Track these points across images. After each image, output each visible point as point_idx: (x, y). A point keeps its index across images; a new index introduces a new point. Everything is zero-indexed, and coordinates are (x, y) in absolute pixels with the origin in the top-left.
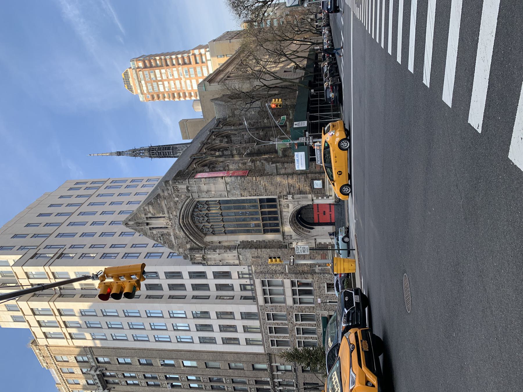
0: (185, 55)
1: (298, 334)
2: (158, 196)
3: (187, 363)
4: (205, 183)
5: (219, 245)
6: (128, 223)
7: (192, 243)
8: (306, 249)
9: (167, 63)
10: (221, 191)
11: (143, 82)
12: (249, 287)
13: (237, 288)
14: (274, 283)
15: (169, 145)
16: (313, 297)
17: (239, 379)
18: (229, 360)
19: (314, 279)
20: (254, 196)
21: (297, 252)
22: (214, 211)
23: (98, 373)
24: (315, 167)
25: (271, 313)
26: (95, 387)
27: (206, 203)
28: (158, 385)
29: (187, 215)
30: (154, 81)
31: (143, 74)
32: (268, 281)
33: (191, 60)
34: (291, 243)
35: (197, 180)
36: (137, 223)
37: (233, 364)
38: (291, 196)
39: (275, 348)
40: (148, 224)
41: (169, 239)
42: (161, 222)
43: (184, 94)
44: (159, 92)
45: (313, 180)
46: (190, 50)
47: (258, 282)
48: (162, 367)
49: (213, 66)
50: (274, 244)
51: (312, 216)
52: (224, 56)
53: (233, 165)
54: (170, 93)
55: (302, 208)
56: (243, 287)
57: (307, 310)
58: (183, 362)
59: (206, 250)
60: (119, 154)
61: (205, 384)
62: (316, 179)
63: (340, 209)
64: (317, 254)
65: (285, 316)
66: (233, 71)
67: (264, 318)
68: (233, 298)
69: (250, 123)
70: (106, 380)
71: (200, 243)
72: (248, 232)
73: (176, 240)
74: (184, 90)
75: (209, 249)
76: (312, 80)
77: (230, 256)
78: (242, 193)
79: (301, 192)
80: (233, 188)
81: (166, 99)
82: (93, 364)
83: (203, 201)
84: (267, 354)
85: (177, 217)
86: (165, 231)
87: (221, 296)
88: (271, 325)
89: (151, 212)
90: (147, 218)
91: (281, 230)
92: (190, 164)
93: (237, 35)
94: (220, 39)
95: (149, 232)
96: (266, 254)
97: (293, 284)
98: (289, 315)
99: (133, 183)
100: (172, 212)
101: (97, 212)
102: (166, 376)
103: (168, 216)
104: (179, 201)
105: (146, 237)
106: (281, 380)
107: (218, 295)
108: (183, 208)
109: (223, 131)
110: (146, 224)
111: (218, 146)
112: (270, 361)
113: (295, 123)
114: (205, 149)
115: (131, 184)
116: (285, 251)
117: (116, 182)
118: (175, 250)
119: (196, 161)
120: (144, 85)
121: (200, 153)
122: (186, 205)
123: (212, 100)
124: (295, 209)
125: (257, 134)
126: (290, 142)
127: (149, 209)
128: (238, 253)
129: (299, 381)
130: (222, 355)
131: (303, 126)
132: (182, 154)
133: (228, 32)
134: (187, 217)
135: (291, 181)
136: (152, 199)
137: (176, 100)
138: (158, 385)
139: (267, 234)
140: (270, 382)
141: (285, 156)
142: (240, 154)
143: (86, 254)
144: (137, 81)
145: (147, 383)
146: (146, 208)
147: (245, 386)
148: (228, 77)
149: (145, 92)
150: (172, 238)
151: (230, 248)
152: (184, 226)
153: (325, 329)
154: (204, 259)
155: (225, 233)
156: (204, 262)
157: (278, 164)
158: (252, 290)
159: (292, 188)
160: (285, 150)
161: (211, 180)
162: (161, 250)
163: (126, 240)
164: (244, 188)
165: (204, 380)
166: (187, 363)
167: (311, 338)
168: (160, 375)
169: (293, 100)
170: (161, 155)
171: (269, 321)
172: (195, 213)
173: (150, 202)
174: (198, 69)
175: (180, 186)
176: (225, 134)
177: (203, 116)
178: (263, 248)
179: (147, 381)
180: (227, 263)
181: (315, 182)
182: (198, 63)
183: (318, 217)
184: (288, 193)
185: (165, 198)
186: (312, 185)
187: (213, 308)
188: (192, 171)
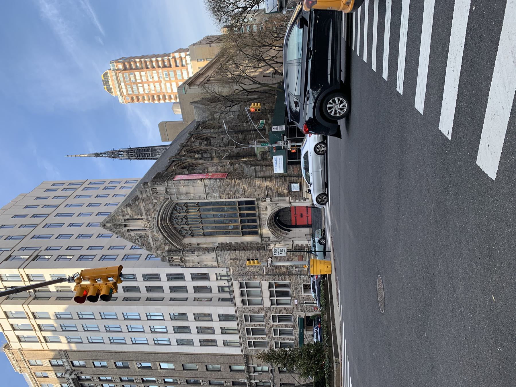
1: (275, 335)
2: (137, 198)
3: (164, 365)
4: (184, 185)
7: (171, 245)
9: (147, 66)
10: (200, 193)
11: (123, 84)
12: (227, 289)
13: (215, 290)
14: (252, 285)
15: (148, 147)
16: (290, 298)
17: (216, 381)
19: (291, 280)
20: (233, 198)
21: (275, 253)
22: (193, 213)
23: (73, 376)
24: (293, 170)
25: (249, 314)
27: (184, 205)
32: (246, 282)
33: (171, 63)
34: (269, 245)
36: (115, 225)
39: (252, 349)
40: (125, 226)
41: (147, 241)
42: (140, 224)
45: (291, 183)
46: (170, 53)
48: (139, 370)
49: (193, 69)
52: (204, 59)
53: (213, 167)
56: (221, 289)
58: (160, 364)
59: (184, 252)
60: (98, 155)
64: (294, 255)
66: (213, 74)
67: (241, 320)
68: (211, 299)
72: (226, 234)
73: (154, 242)
74: (163, 93)
77: (209, 258)
79: (279, 195)
81: (146, 102)
82: (68, 368)
85: (156, 219)
86: (143, 233)
87: (199, 298)
88: (248, 326)
90: (125, 220)
91: (259, 232)
92: (170, 166)
94: (200, 43)
95: (127, 234)
97: (270, 285)
98: (267, 316)
101: (74, 213)
102: (142, 379)
103: (146, 218)
104: (158, 203)
105: (124, 238)
106: (257, 381)
107: (196, 297)
108: (162, 210)
109: (202, 134)
110: (123, 226)
113: (273, 127)
115: (110, 185)
116: (263, 253)
117: (94, 183)
120: (124, 87)
121: (179, 155)
122: (165, 207)
123: (192, 103)
125: (237, 137)
128: (216, 255)
133: (208, 36)
134: (165, 219)
136: (130, 201)
139: (245, 236)
140: (247, 383)
141: (263, 159)
142: (219, 157)
144: (116, 82)
148: (208, 80)
149: (125, 94)
150: (150, 240)
151: (209, 250)
152: (163, 228)
153: (301, 330)
154: (182, 261)
155: (204, 235)
156: (183, 264)
157: (256, 167)
158: (230, 292)
159: (270, 191)
160: (263, 154)
161: (191, 182)
162: (139, 252)
163: (105, 242)
164: (223, 190)
165: (181, 382)
166: (164, 365)
167: (288, 338)
169: (271, 105)
170: (140, 157)
171: (247, 323)
173: (128, 203)
174: (178, 72)
177: (183, 118)
178: (241, 250)
179: (123, 384)
182: (178, 67)
183: (296, 219)
184: (266, 195)
185: (144, 200)
186: (289, 188)
187: (190, 310)
188: (171, 174)
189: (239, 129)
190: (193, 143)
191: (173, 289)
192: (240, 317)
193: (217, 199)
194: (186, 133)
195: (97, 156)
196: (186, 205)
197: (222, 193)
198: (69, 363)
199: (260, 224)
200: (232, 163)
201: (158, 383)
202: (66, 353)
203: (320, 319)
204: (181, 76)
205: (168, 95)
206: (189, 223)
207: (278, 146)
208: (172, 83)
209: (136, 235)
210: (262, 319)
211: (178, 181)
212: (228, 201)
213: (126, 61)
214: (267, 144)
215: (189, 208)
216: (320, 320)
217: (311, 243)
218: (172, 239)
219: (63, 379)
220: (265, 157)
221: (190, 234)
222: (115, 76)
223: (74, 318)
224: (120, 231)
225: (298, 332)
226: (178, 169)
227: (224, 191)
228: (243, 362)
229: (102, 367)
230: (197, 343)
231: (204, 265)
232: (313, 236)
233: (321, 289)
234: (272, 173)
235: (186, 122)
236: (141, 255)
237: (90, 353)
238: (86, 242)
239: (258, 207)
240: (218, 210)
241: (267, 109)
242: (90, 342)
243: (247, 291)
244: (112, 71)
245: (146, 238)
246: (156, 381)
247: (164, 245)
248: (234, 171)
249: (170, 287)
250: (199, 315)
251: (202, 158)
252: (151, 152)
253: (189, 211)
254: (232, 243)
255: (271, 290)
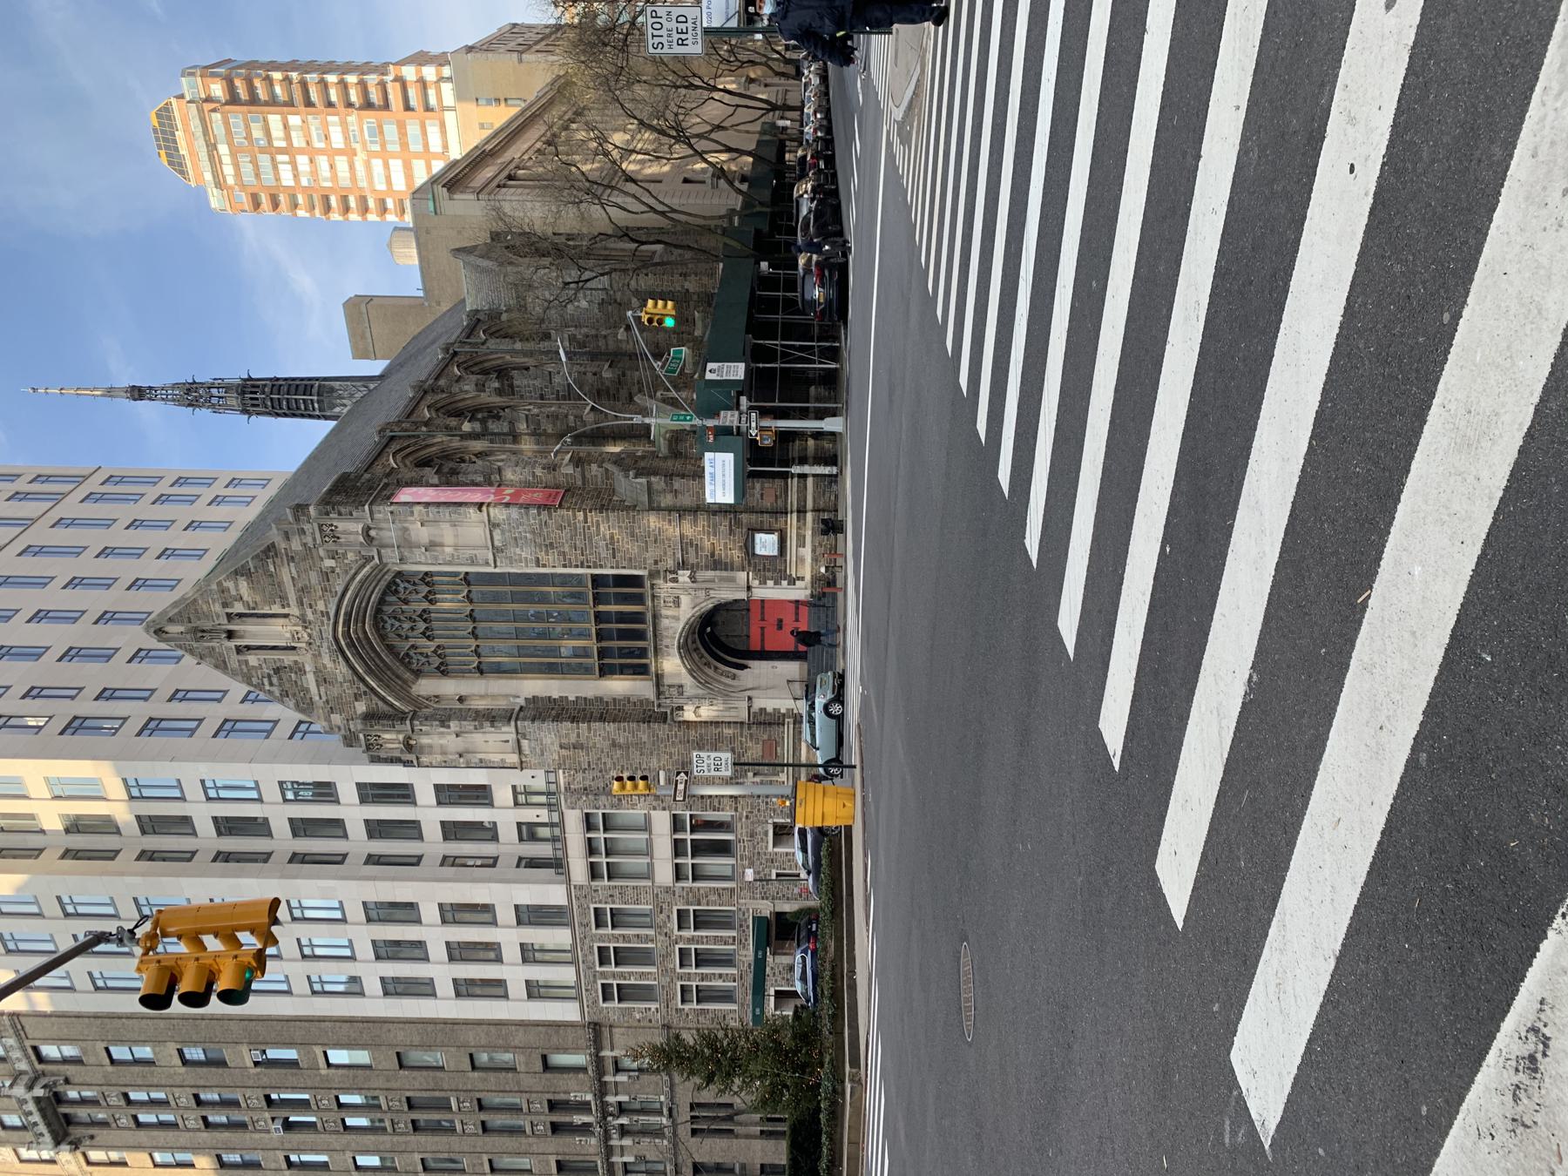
0: (372, 79)
1: (682, 965)
2: (270, 550)
3: (338, 1056)
4: (425, 518)
5: (459, 706)
6: (166, 629)
7: (373, 697)
8: (690, 25)
9: (309, 97)
10: (474, 547)
11: (223, 149)
12: (544, 832)
13: (508, 833)
14: (619, 821)
15: (310, 379)
16: (731, 861)
17: (497, 1099)
18: (473, 1044)
19: (739, 809)
20: (577, 566)
21: (699, 769)
22: (448, 603)
23: (39, 1092)
24: (762, 495)
25: (608, 907)
26: (29, 1136)
27: (422, 579)
28: (242, 1126)
29: (361, 614)
30: (262, 151)
31: (226, 123)
32: (604, 814)
33: (391, 97)
34: (681, 708)
35: (401, 509)
36: (196, 630)
37: (486, 1055)
38: (688, 573)
39: (606, 932)
40: (231, 635)
41: (299, 683)
42: (277, 632)
43: (363, 201)
44: (279, 187)
45: (754, 530)
46: (387, 64)
47: (573, 819)
48: (258, 1070)
49: (462, 128)
50: (629, 707)
51: (745, 633)
52: (498, 100)
53: (517, 469)
54: (315, 196)
55: (721, 608)
56: (528, 832)
57: (713, 898)
58: (325, 1053)
59: (416, 722)
60: (138, 393)
61: (394, 1116)
62: (761, 530)
63: (823, 617)
64: (751, 740)
65: (646, 915)
66: (526, 157)
67: (585, 922)
68: (493, 862)
69: (575, 335)
70: (66, 1116)
71: (398, 699)
72: (552, 670)
73: (322, 689)
74: (360, 189)
75: (426, 719)
76: (766, 229)
77: (494, 742)
78: (542, 555)
79: (717, 564)
80: (513, 542)
81: (301, 213)
82: (23, 1066)
83: (415, 572)
84: (589, 1023)
85: (329, 619)
86: (288, 659)
87: (456, 857)
88: (604, 941)
89: (245, 598)
90: (229, 616)
91: (653, 669)
92: (379, 454)
93: (542, 39)
94: (486, 47)
95: (233, 661)
96: (604, 739)
97: (677, 823)
98: (661, 912)
99: (182, 488)
100: (313, 603)
101: (53, 578)
102: (267, 1098)
103: (297, 613)
104: (338, 570)
105: (225, 673)
106: (624, 1098)
107: (448, 853)
108: (350, 592)
109: (486, 354)
110: (224, 635)
111: (469, 402)
112: (597, 1043)
113: (710, 366)
114: (429, 407)
115: (176, 490)
116: (662, 730)
117: (122, 480)
118: (319, 717)
119: (398, 448)
120: (226, 160)
121: (413, 418)
122: (359, 582)
123: (458, 251)
124: (698, 611)
125: (595, 374)
126: (692, 423)
127: (237, 590)
128: (517, 733)
129: (676, 1100)
130: (474, 1147)
131: (732, 378)
132: (349, 411)
133: (515, 25)
134: (360, 618)
135: (688, 529)
136: (249, 559)
137: (332, 219)
138: (242, 1126)
139: (609, 679)
140: (593, 1103)
141: (675, 454)
142: (540, 435)
143: (11, 717)
144: (201, 142)
145: (205, 1119)
146: (230, 584)
147: (518, 1119)
148: (510, 178)
149: (230, 181)
150: (310, 681)
151: (494, 717)
152: (351, 645)
153: (760, 953)
154: (409, 747)
155: (480, 671)
156: (410, 754)
157: (653, 479)
158: (554, 839)
159: (692, 551)
160: (677, 437)
161: (445, 511)
162: (273, 710)
163: (158, 675)
164: (547, 542)
165: (391, 1104)
166: (338, 1056)
167: (720, 976)
168: (248, 1093)
169: (705, 280)
170: (281, 408)
171: (601, 931)
172: (385, 608)
173: (242, 566)
174: (413, 129)
175: (342, 526)
176: (494, 362)
177: (425, 289)
178: (595, 721)
179: (204, 1113)
180: (481, 761)
181: (760, 538)
182: (413, 110)
183: (763, 635)
184: (679, 563)
185: (292, 557)
186: (749, 547)
187: (429, 894)
188: (385, 480)
189: (603, 347)
190: (457, 381)
191: (376, 829)
192: (580, 915)
193: (527, 566)
194: (433, 342)
195: (137, 396)
196: (428, 579)
197: (544, 549)
198: (24, 1049)
199: (655, 648)
200: (580, 458)
201: (316, 1108)
202: (16, 1021)
203: (814, 926)
204: (421, 141)
205: (375, 200)
206: (435, 632)
207: (721, 424)
208: (391, 162)
209: (264, 665)
210: (648, 919)
211: (407, 508)
212: (561, 575)
213: (238, 75)
214: (688, 418)
215: (437, 588)
216: (814, 929)
217: (802, 707)
218: (379, 679)
219: (5, 1099)
220: (681, 447)
221: (436, 665)
222: (197, 121)
223: (77, 988)
224: (213, 648)
225: (751, 958)
226: (406, 466)
227: (551, 544)
228: (582, 1043)
229: (137, 1062)
230: (445, 988)
231: (477, 761)
232: (809, 693)
233: (823, 862)
234: (698, 498)
235: (434, 304)
236: (276, 722)
237: (99, 1021)
238: (93, 675)
239: (653, 596)
240: (528, 598)
241: (691, 290)
242: (97, 989)
243: (605, 839)
244: (189, 102)
245: (296, 673)
246: (313, 1102)
247: (352, 699)
248: (584, 484)
249: (367, 821)
250: (462, 945)
251: (484, 435)
252: (318, 395)
253: (438, 596)
254: (567, 697)
255: (679, 836)
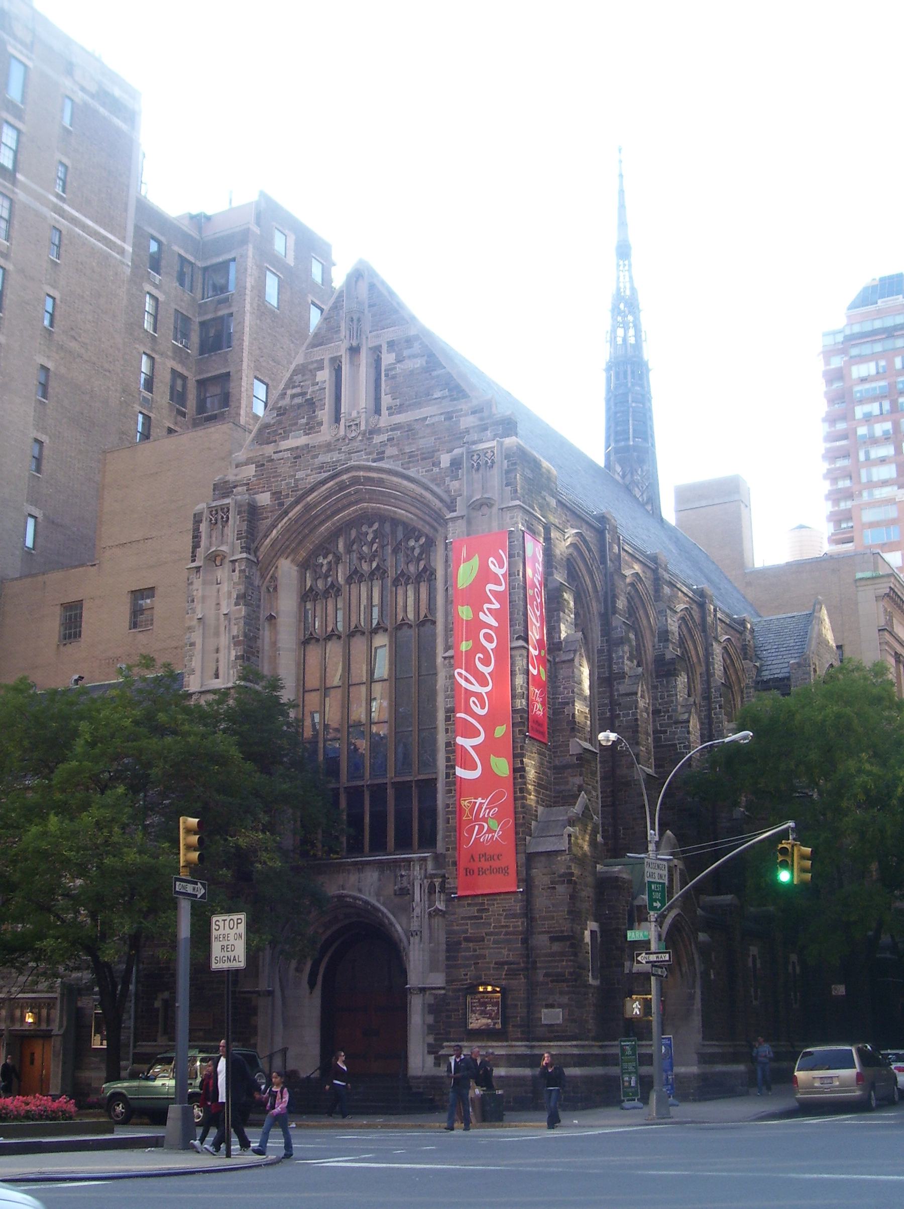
21: (221, 924)
40: (354, 351)
73: (287, 455)
86: (324, 414)
89: (398, 365)
92: (579, 517)
108: (315, 494)
127: (409, 357)
150: (297, 440)
151: (248, 659)
152: (342, 487)
209: (317, 387)
224: (338, 332)
245: (307, 424)
